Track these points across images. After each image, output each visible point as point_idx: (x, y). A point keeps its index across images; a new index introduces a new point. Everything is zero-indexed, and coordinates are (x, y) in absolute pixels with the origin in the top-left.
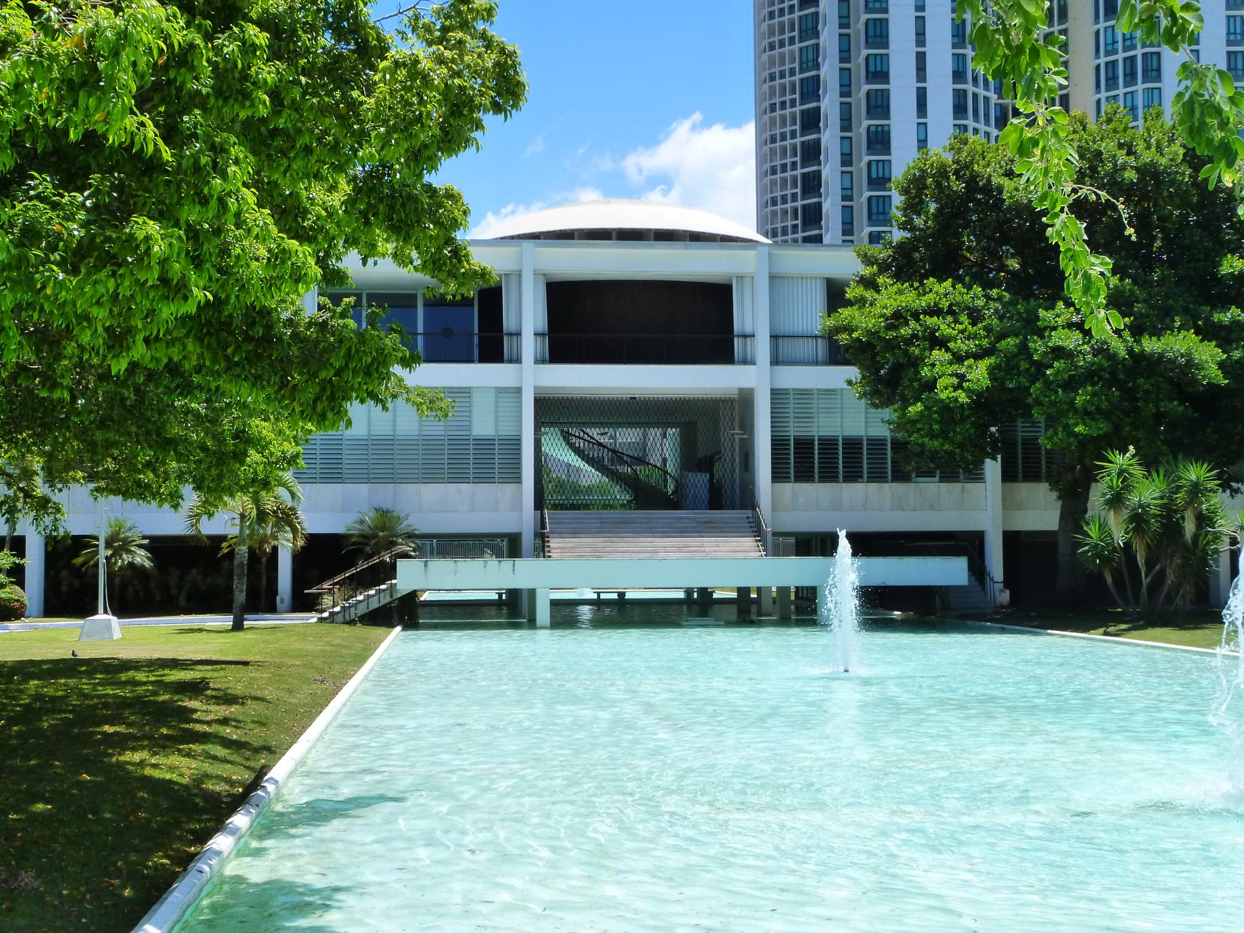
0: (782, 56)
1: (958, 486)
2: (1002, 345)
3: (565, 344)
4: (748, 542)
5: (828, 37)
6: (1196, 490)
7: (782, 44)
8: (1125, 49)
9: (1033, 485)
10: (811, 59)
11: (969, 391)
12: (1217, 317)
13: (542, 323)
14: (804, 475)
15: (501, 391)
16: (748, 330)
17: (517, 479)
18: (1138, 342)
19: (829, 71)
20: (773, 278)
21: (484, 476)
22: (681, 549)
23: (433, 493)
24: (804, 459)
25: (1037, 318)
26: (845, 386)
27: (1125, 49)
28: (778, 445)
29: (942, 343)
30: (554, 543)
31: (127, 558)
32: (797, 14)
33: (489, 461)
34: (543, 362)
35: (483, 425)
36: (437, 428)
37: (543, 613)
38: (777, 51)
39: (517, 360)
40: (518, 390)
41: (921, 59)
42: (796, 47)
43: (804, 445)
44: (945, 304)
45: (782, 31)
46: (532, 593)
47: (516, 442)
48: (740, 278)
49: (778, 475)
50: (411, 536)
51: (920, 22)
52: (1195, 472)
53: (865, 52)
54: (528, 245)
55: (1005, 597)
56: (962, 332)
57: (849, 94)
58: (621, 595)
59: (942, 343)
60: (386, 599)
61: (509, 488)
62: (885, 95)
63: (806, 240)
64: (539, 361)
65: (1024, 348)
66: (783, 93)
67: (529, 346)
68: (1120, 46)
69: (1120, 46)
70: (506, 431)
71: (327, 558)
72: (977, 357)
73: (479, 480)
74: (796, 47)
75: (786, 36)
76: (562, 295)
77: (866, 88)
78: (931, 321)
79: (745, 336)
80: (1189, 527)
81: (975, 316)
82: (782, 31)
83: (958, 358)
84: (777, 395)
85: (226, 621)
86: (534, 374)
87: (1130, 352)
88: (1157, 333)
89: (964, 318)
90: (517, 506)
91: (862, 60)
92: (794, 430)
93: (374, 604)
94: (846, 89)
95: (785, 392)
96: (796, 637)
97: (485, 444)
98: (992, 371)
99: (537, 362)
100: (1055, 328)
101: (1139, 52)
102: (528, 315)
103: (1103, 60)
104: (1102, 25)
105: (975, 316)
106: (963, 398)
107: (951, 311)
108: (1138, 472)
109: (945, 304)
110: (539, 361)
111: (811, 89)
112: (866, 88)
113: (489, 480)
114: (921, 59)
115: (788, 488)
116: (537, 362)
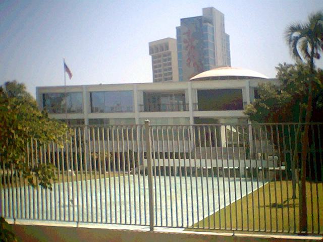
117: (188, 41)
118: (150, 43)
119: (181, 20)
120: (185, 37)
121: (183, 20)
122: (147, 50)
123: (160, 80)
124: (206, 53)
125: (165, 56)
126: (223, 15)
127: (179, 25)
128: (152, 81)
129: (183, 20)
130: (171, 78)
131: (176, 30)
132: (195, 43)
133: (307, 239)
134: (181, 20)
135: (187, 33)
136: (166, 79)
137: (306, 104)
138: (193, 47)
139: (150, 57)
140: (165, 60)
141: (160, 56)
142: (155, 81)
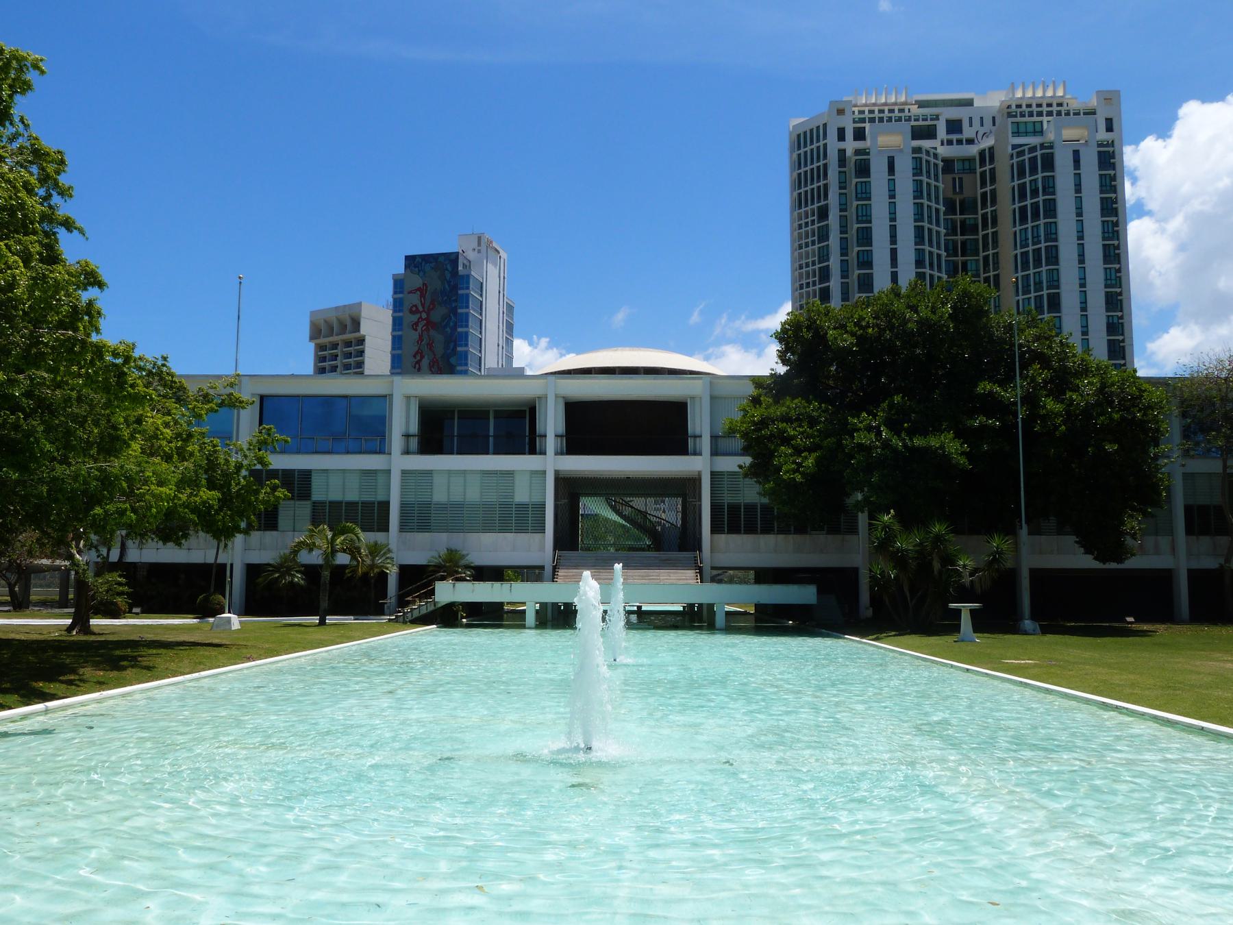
0: (807, 253)
1: (839, 537)
2: (825, 443)
3: (574, 443)
4: (691, 573)
5: (834, 241)
6: (938, 538)
7: (807, 245)
8: (1034, 244)
9: (767, 536)
10: (824, 255)
11: (803, 474)
12: (969, 423)
13: (561, 429)
14: (734, 529)
15: (534, 473)
16: (698, 432)
17: (543, 530)
18: (911, 439)
19: (834, 263)
20: (712, 398)
21: (521, 529)
22: (643, 577)
23: (488, 538)
24: (731, 519)
25: (848, 424)
26: (737, 469)
27: (1034, 244)
28: (716, 509)
29: (786, 441)
30: (561, 572)
31: (288, 579)
32: (816, 226)
33: (523, 518)
34: (562, 454)
35: (522, 495)
36: (492, 497)
37: (530, 618)
38: (804, 250)
39: (696, 453)
40: (544, 472)
41: (894, 253)
42: (817, 246)
43: (734, 509)
44: (793, 414)
45: (807, 237)
46: (711, 606)
47: (542, 506)
48: (693, 398)
49: (716, 529)
50: (467, 567)
51: (893, 230)
52: (937, 528)
53: (856, 249)
54: (552, 378)
55: (869, 613)
56: (802, 433)
57: (847, 277)
58: (639, 608)
59: (786, 441)
60: (431, 608)
61: (537, 536)
62: (870, 276)
63: (356, 373)
64: (559, 453)
65: (839, 444)
66: (808, 277)
67: (551, 443)
68: (1030, 241)
69: (1030, 241)
70: (536, 499)
71: (418, 579)
72: (810, 450)
73: (518, 531)
74: (817, 246)
75: (810, 240)
76: (576, 411)
77: (857, 272)
78: (782, 425)
79: (695, 437)
80: (936, 565)
81: (813, 422)
82: (807, 237)
83: (798, 451)
84: (714, 475)
85: (315, 619)
86: (553, 462)
87: (905, 446)
88: (925, 433)
89: (805, 424)
90: (542, 549)
91: (855, 254)
92: (727, 499)
93: (424, 611)
94: (845, 274)
95: (721, 473)
96: (554, 638)
97: (522, 507)
98: (818, 461)
99: (556, 454)
100: (858, 430)
101: (1043, 245)
102: (552, 423)
103: (1019, 251)
104: (1018, 228)
105: (813, 422)
106: (798, 478)
107: (798, 419)
108: (896, 527)
109: (793, 414)
110: (559, 453)
111: (825, 274)
112: (857, 272)
113: (525, 531)
114: (894, 253)
115: (722, 538)
116: (556, 454)
117: (421, 309)
118: (312, 313)
119: (407, 258)
120: (415, 299)
121: (411, 261)
122: (306, 331)
123: (334, 369)
124: (464, 320)
125: (348, 344)
126: (576, 611)
127: (400, 269)
128: (310, 370)
129: (411, 261)
130: (360, 365)
131: (391, 282)
132: (436, 316)
133: (700, 499)
134: (407, 258)
135: (419, 289)
136: (347, 367)
137: (793, 354)
138: (430, 324)
139: (311, 346)
140: (349, 355)
141: (335, 346)
142: (321, 371)
